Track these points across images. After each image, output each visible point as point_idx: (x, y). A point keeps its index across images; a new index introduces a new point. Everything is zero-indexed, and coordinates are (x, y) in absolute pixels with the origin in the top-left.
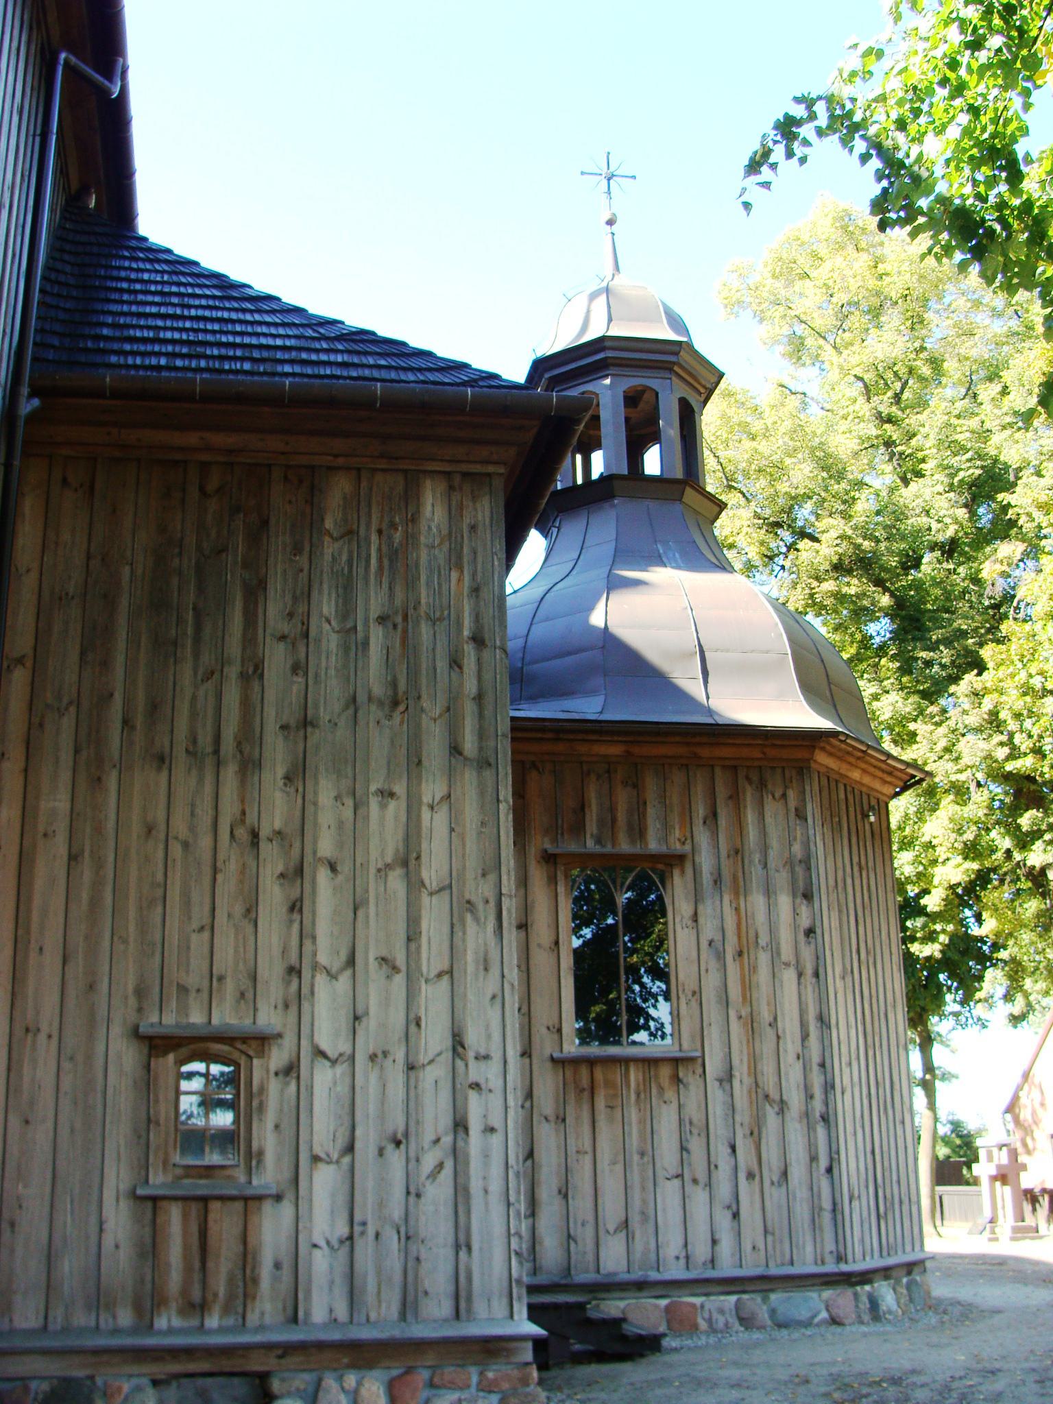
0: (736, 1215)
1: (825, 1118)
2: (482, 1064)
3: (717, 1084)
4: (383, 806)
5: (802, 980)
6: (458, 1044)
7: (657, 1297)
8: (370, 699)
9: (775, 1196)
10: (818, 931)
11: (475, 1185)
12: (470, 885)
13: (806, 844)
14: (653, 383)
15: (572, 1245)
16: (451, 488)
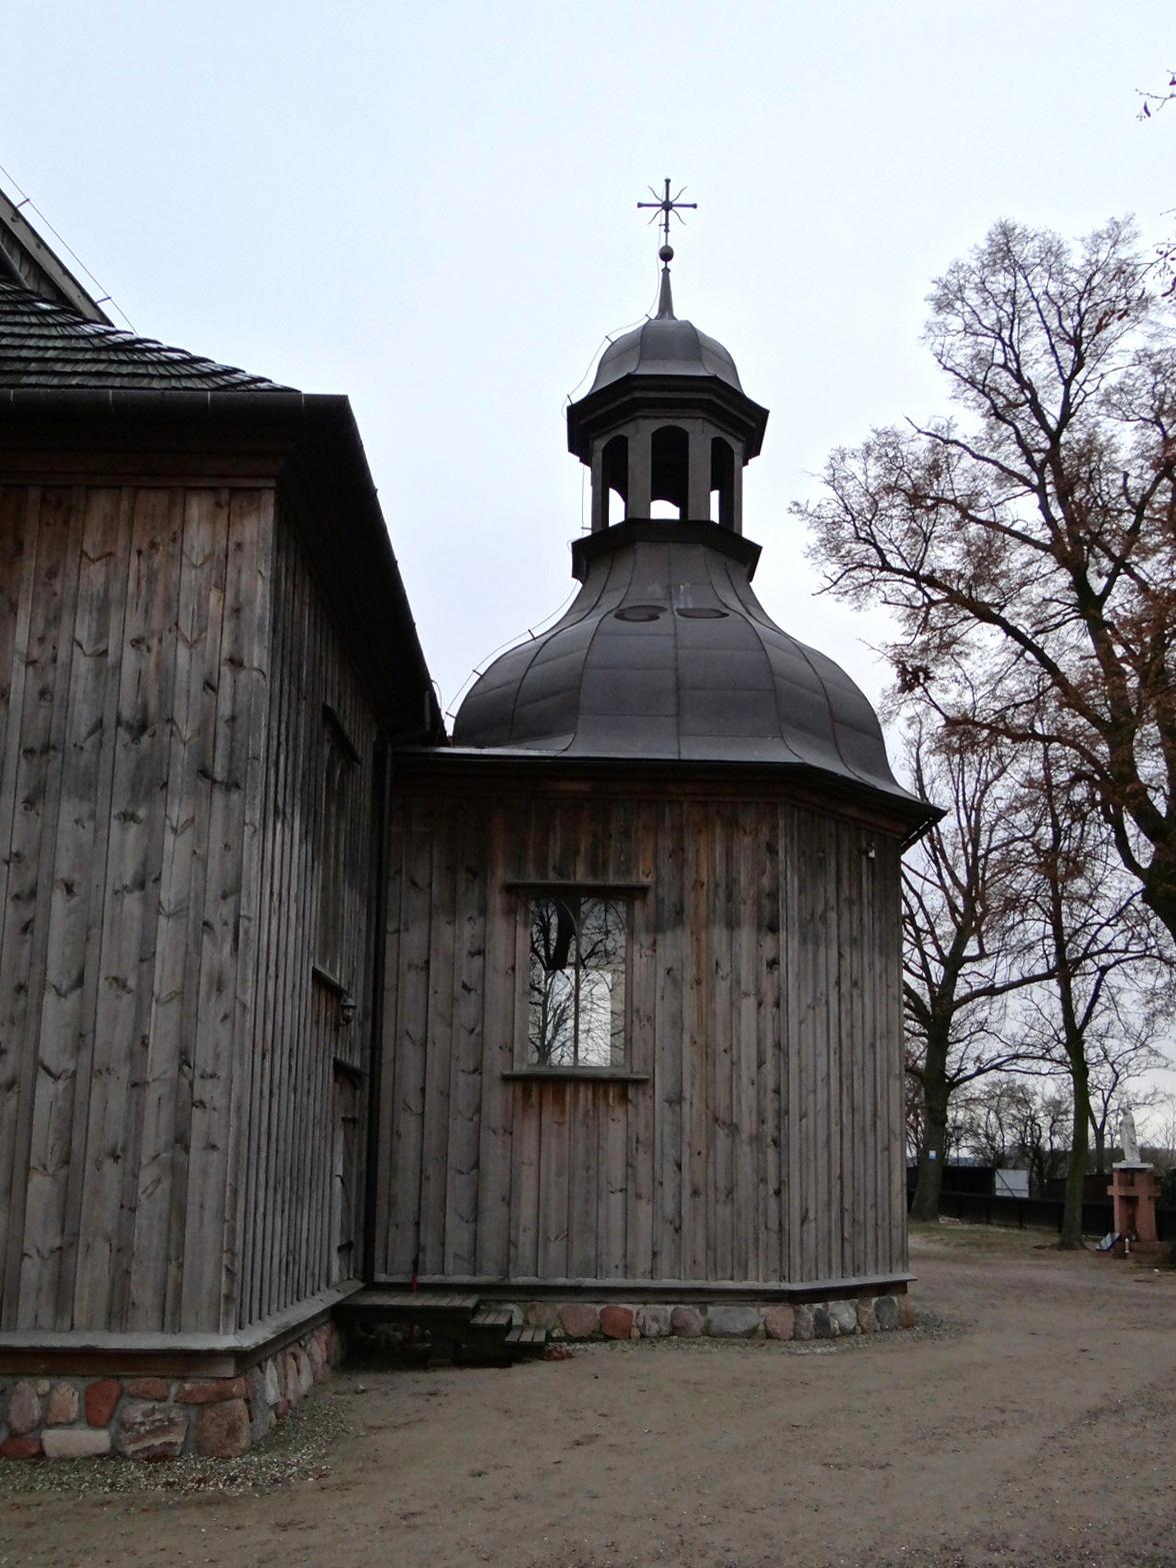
0: (678, 1230)
1: (776, 1142)
2: (209, 1083)
3: (667, 1105)
4: (124, 830)
5: (762, 1010)
6: (184, 1058)
7: (597, 1303)
8: (119, 722)
9: (724, 1212)
10: (782, 963)
11: (193, 1198)
12: (210, 906)
13: (775, 878)
14: (680, 423)
15: (512, 1248)
16: (218, 505)
